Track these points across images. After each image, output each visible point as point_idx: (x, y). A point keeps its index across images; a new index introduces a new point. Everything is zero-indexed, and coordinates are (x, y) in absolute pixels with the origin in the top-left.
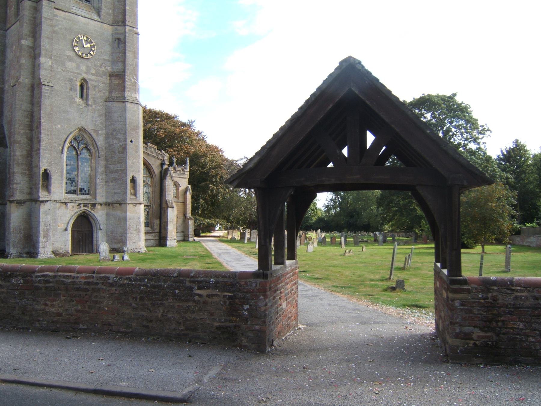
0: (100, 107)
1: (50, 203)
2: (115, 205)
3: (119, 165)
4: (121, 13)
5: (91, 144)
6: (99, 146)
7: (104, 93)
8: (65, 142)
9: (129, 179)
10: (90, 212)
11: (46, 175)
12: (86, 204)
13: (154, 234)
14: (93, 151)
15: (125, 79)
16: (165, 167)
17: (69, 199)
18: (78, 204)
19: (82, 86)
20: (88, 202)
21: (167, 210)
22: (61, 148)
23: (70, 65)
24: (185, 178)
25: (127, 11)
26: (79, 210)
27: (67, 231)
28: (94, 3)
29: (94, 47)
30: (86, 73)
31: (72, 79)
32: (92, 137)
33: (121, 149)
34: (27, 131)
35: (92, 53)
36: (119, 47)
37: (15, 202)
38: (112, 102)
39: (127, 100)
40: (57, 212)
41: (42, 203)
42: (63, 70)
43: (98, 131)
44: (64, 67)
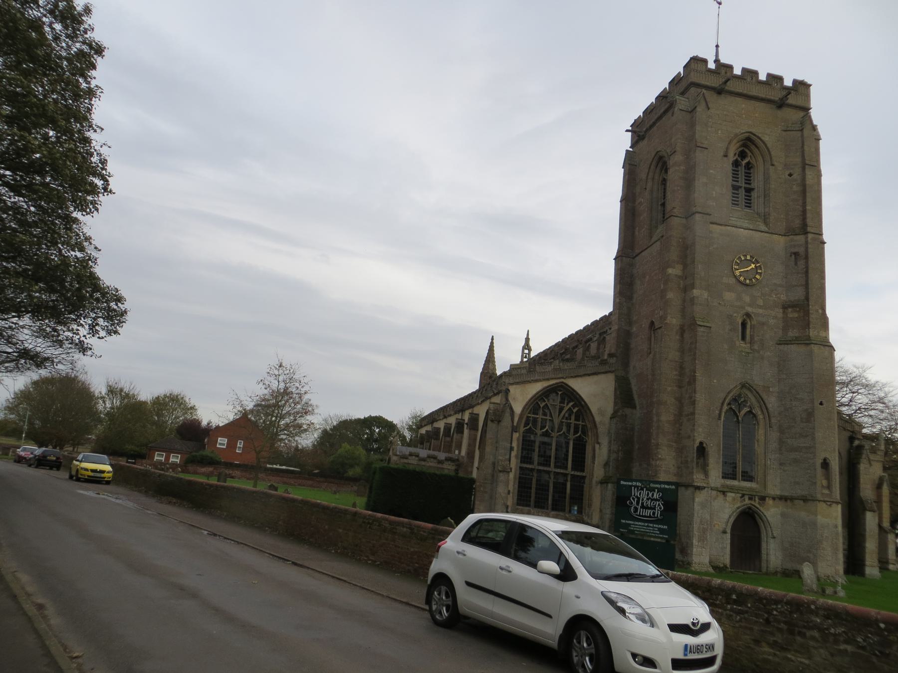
1: (708, 491)
2: (796, 502)
5: (758, 407)
6: (770, 409)
8: (723, 404)
9: (819, 461)
10: (757, 508)
11: (702, 450)
12: (753, 495)
14: (761, 417)
15: (809, 310)
17: (727, 486)
18: (740, 495)
20: (755, 494)
21: (864, 514)
22: (717, 412)
23: (729, 296)
25: (808, 211)
26: (743, 504)
28: (757, 209)
29: (761, 269)
30: (750, 305)
31: (731, 316)
34: (675, 388)
35: (758, 277)
36: (796, 264)
38: (789, 346)
39: (813, 342)
41: (697, 491)
42: (720, 304)
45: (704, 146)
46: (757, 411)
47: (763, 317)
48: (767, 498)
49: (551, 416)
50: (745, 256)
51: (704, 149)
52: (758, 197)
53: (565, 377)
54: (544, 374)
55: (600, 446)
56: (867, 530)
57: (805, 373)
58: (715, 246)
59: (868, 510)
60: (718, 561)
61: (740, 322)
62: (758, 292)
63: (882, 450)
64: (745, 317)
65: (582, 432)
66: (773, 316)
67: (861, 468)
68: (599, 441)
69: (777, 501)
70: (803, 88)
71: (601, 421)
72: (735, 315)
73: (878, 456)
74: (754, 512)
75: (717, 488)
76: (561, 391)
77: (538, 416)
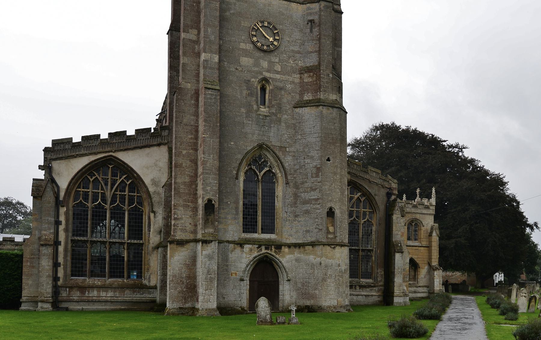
2: (307, 247)
3: (312, 193)
5: (276, 166)
7: (292, 97)
8: (240, 164)
10: (273, 256)
12: (269, 245)
13: (376, 289)
14: (279, 175)
16: (393, 197)
18: (257, 246)
19: (263, 89)
20: (271, 243)
22: (235, 172)
23: (246, 61)
24: (430, 214)
26: (260, 253)
30: (268, 71)
31: (249, 81)
33: (314, 171)
35: (276, 43)
36: (311, 31)
38: (304, 108)
40: (230, 256)
42: (237, 69)
43: (286, 148)
46: (276, 170)
47: (281, 82)
48: (283, 247)
49: (102, 189)
50: (262, 22)
53: (113, 151)
55: (155, 214)
56: (396, 267)
57: (316, 133)
58: (232, 12)
60: (236, 305)
61: (259, 88)
63: (434, 205)
65: (137, 202)
67: (394, 218)
68: (154, 210)
69: (292, 248)
71: (155, 192)
72: (253, 80)
73: (430, 211)
74: (271, 260)
75: (234, 241)
76: (113, 164)
77: (89, 190)
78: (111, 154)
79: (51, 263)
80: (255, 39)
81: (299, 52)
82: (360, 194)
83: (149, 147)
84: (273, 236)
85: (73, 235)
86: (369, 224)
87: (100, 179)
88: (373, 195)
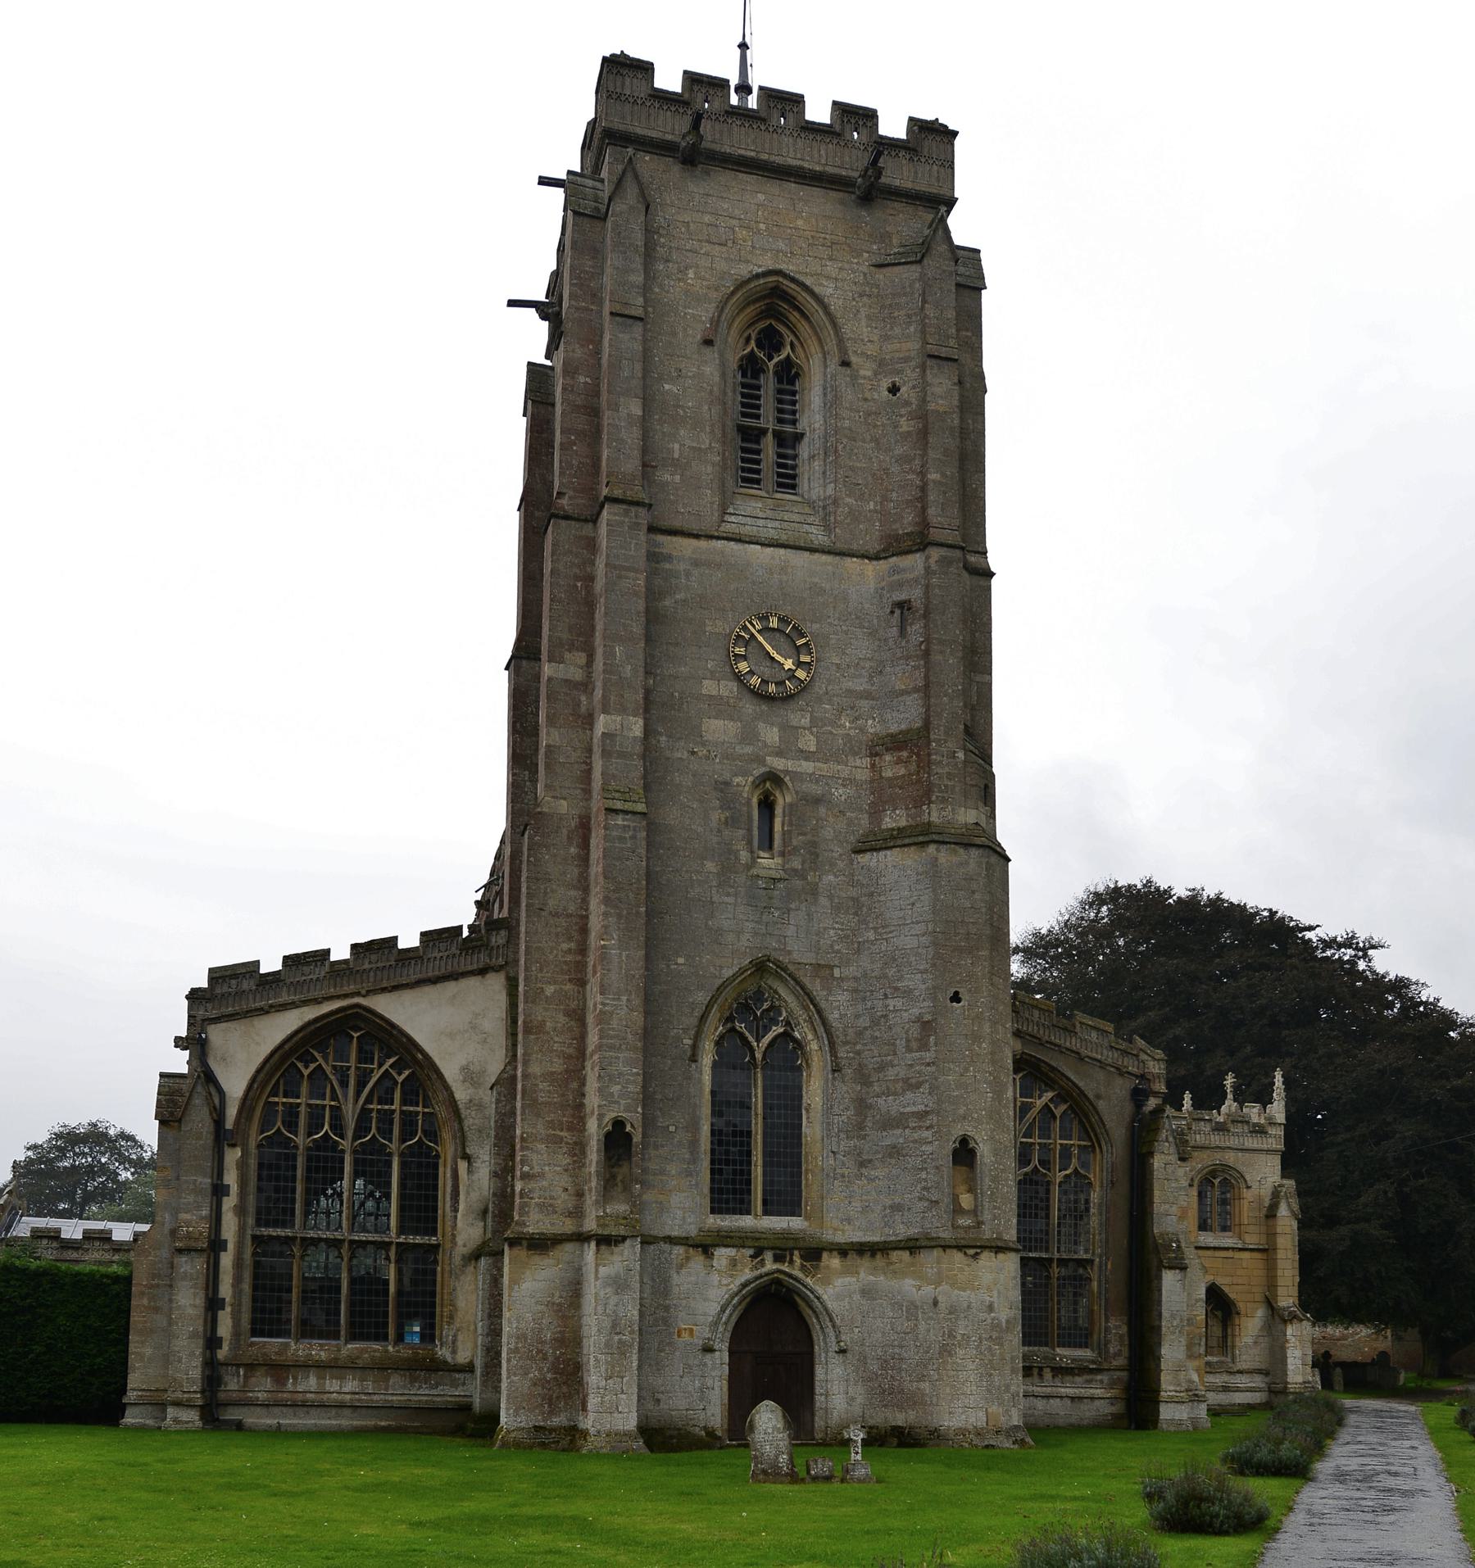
0: (836, 876)
2: (895, 1255)
4: (908, 502)
5: (805, 1021)
7: (850, 823)
8: (703, 1018)
10: (796, 1279)
12: (785, 1250)
13: (1105, 1377)
14: (814, 1046)
16: (1152, 1103)
18: (751, 1252)
20: (791, 1244)
23: (718, 729)
24: (1268, 1151)
26: (758, 1273)
27: (709, 1356)
30: (780, 753)
31: (727, 784)
32: (807, 994)
33: (915, 1031)
35: (805, 658)
36: (903, 632)
37: (525, 1243)
38: (882, 853)
42: (693, 753)
43: (831, 968)
44: (699, 739)
45: (633, 313)
47: (817, 781)
48: (825, 1255)
49: (334, 1097)
51: (630, 321)
52: (812, 457)
53: (363, 992)
54: (306, 988)
56: (1165, 1314)
59: (1166, 1268)
61: (755, 801)
62: (803, 716)
64: (768, 785)
65: (424, 1132)
66: (844, 779)
67: (1156, 1165)
68: (468, 1151)
69: (852, 1256)
70: (934, 144)
71: (471, 1101)
72: (737, 780)
73: (1270, 1140)
74: (791, 1291)
75: (687, 1238)
76: (361, 1029)
77: (299, 1101)
78: (356, 1000)
79: (200, 1301)
80: (743, 666)
81: (867, 695)
82: (1050, 1095)
83: (456, 979)
84: (795, 1223)
85: (259, 1223)
86: (1079, 1183)
87: (328, 1070)
88: (1091, 1096)
